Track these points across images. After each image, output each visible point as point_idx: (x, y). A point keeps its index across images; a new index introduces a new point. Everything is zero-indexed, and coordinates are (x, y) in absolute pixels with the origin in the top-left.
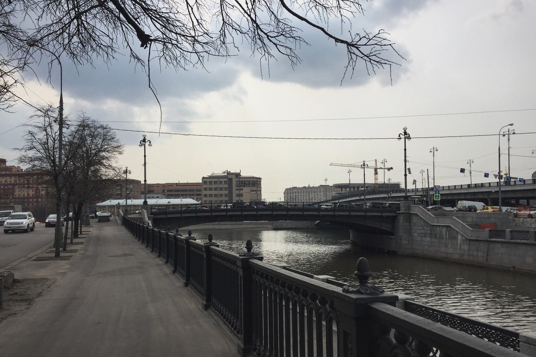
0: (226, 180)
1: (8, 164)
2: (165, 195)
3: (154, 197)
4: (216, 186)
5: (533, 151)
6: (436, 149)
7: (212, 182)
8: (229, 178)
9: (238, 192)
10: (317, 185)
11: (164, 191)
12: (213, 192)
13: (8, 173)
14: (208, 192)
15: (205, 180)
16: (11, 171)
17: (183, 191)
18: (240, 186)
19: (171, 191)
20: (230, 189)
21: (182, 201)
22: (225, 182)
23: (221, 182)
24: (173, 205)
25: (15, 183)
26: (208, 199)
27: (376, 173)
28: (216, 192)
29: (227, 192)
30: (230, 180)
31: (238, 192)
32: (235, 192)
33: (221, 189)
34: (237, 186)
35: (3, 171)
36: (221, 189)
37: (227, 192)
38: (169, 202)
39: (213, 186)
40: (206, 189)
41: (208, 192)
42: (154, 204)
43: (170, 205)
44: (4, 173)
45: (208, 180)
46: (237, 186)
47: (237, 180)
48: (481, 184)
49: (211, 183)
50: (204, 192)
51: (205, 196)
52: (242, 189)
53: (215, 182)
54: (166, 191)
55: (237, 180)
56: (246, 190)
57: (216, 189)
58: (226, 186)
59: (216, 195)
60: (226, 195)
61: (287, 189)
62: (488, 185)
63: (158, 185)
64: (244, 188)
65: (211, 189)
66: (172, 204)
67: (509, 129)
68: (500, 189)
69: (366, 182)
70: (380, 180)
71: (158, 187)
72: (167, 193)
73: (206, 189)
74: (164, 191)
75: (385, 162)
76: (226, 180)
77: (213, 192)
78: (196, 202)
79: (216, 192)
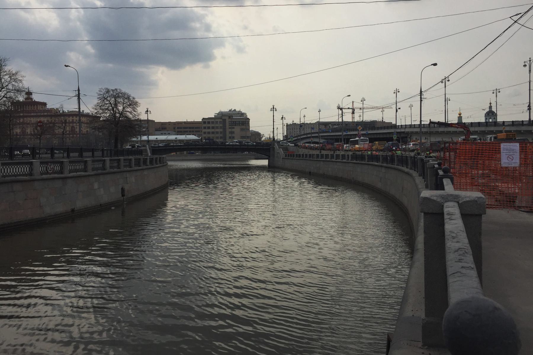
0: (221, 120)
1: (49, 106)
2: (175, 131)
3: (166, 134)
4: (213, 125)
5: (493, 91)
6: (448, 79)
7: (218, 122)
8: (223, 119)
9: (230, 130)
10: (314, 122)
11: (174, 128)
12: (211, 130)
13: (49, 114)
14: (207, 130)
15: (205, 120)
16: (52, 112)
17: (190, 128)
18: (232, 126)
19: (181, 128)
20: (224, 128)
21: (186, 137)
22: (220, 122)
23: (217, 122)
24: (179, 140)
25: (48, 123)
26: (207, 136)
27: (353, 113)
28: (213, 130)
29: (221, 130)
30: (224, 120)
31: (230, 130)
32: (228, 130)
33: (217, 128)
34: (229, 125)
35: (46, 112)
36: (217, 128)
37: (221, 130)
38: (157, 139)
39: (211, 125)
40: (205, 128)
41: (207, 130)
42: (165, 139)
43: (177, 140)
44: (46, 114)
45: (207, 121)
46: (229, 125)
47: (230, 120)
48: (511, 122)
49: (209, 123)
50: (204, 130)
51: (205, 133)
52: (234, 128)
53: (212, 122)
54: (176, 128)
55: (230, 120)
56: (237, 129)
57: (213, 128)
58: (221, 125)
59: (213, 133)
60: (221, 132)
61: (203, 118)
62: (400, 127)
63: (170, 123)
64: (235, 127)
65: (209, 128)
66: (179, 139)
67: (530, 58)
68: (421, 130)
69: (149, 139)
70: (357, 119)
71: (169, 124)
72: (177, 130)
73: (205, 128)
74: (174, 128)
75: (397, 92)
76: (221, 120)
77: (211, 130)
78: (198, 138)
79: (213, 130)
